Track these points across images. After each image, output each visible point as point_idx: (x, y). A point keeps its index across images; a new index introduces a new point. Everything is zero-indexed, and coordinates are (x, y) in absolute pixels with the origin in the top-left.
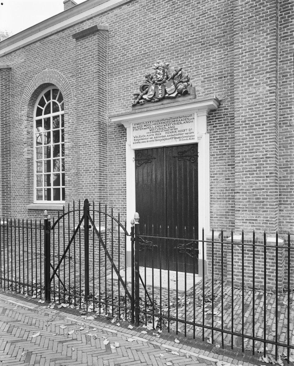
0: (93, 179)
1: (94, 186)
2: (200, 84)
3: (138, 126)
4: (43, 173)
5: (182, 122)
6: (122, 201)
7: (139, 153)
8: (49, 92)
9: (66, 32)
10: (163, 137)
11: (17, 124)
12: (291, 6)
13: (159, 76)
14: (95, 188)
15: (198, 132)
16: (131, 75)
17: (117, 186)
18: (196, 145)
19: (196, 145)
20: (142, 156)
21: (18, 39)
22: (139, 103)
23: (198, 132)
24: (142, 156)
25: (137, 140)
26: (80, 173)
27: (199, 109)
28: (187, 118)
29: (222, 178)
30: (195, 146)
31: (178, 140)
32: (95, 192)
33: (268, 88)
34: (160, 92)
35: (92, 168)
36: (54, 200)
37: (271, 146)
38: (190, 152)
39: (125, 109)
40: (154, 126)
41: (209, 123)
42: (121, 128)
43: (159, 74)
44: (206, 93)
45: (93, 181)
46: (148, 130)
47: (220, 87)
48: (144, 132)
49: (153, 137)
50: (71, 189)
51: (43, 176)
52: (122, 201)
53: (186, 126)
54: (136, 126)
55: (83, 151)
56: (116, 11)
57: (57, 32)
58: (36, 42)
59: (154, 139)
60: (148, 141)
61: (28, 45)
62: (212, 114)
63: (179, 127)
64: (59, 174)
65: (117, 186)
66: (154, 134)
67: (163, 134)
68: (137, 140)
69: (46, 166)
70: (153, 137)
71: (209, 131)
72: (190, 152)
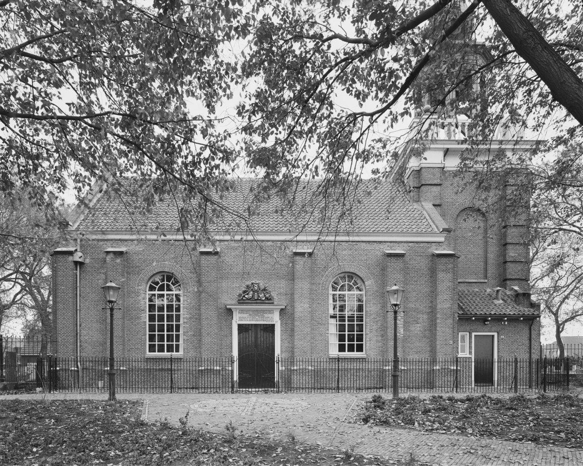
3: (242, 311)
7: (240, 327)
8: (332, 285)
11: (133, 295)
15: (275, 319)
18: (274, 325)
19: (274, 325)
20: (242, 328)
22: (241, 301)
23: (275, 319)
24: (242, 328)
25: (238, 319)
28: (271, 311)
29: (286, 342)
30: (274, 325)
36: (159, 351)
37: (309, 330)
41: (280, 315)
42: (230, 312)
44: (280, 301)
53: (270, 315)
62: (282, 311)
63: (266, 315)
64: (163, 305)
68: (240, 319)
71: (280, 319)
72: (270, 329)
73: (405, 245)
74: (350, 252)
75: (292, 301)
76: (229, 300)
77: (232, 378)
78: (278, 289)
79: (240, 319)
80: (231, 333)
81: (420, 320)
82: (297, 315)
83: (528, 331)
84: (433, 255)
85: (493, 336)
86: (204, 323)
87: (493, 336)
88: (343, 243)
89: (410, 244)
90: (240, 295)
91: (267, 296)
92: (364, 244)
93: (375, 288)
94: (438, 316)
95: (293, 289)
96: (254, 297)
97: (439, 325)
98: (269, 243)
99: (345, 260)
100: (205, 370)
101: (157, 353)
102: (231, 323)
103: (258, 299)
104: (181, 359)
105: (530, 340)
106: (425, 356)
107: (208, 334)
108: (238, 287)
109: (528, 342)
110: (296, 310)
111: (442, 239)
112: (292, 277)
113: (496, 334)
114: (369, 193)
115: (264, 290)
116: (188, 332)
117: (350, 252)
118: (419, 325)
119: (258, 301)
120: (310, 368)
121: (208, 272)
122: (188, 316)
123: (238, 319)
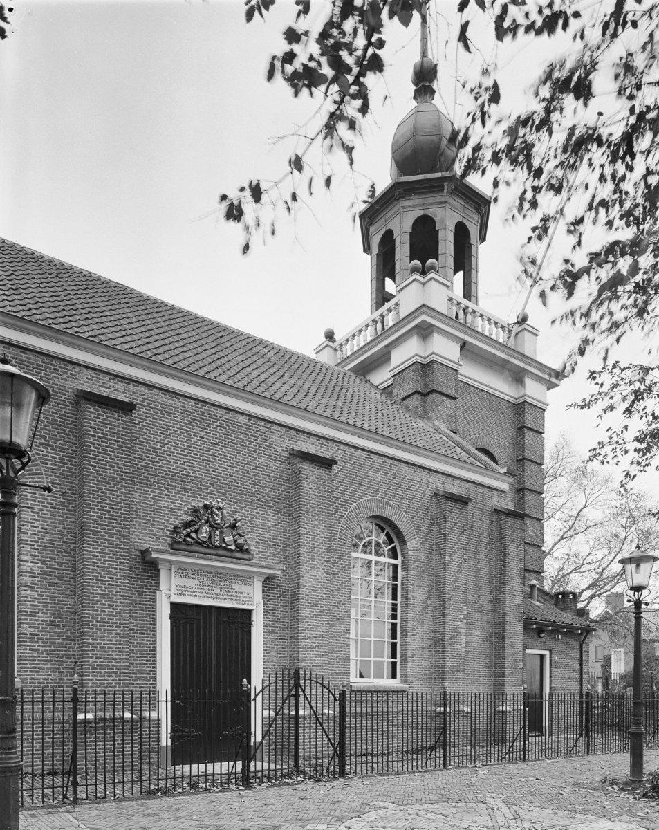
0: (116, 637)
1: (120, 648)
2: (254, 543)
3: (184, 570)
4: (372, 659)
5: (241, 582)
6: (147, 674)
9: (29, 355)
10: (216, 594)
12: (40, 432)
13: (216, 518)
14: (119, 652)
16: (166, 495)
17: (138, 650)
21: (286, 411)
22: (174, 546)
23: (252, 598)
25: (174, 589)
26: (89, 625)
27: (261, 574)
28: (247, 578)
30: (249, 612)
31: (234, 602)
32: (120, 659)
33: (325, 575)
34: (217, 538)
35: (114, 621)
38: (243, 618)
39: (155, 539)
40: (205, 578)
42: (148, 568)
43: (217, 515)
45: (116, 641)
46: (197, 582)
47: (274, 555)
48: (192, 583)
49: (204, 592)
50: (36, 650)
51: (372, 663)
52: (147, 674)
53: (245, 589)
54: (180, 571)
55: (97, 590)
56: (142, 389)
57: (165, 391)
58: (242, 414)
59: (204, 595)
60: (196, 596)
61: (213, 405)
62: (268, 581)
63: (237, 587)
65: (138, 650)
66: (205, 588)
67: (217, 590)
69: (390, 649)
70: (204, 592)
73: (462, 484)
74: (385, 478)
75: (295, 564)
76: (150, 537)
77: (159, 741)
78: (260, 528)
79: (181, 590)
80: (154, 620)
81: (479, 624)
82: (305, 593)
83: (577, 650)
84: (496, 511)
85: (542, 657)
86: (93, 590)
87: (542, 657)
88: (376, 457)
89: (468, 485)
90: (175, 530)
91: (241, 541)
92: (405, 468)
93: (422, 558)
94: (508, 618)
95: (298, 535)
96: (200, 536)
97: (508, 634)
98: (242, 419)
99: (377, 491)
100: (96, 721)
101: (372, 679)
102: (154, 600)
103: (220, 547)
104: (404, 691)
105: (581, 664)
106: (483, 689)
107: (103, 623)
108: (178, 507)
109: (578, 666)
110: (302, 583)
111: (505, 487)
112: (290, 507)
113: (547, 653)
114: (626, 452)
115: (234, 527)
116: (34, 613)
117: (385, 478)
118: (477, 632)
119: (221, 551)
120: (128, 715)
121: (104, 453)
122: (36, 568)
123: (174, 589)
